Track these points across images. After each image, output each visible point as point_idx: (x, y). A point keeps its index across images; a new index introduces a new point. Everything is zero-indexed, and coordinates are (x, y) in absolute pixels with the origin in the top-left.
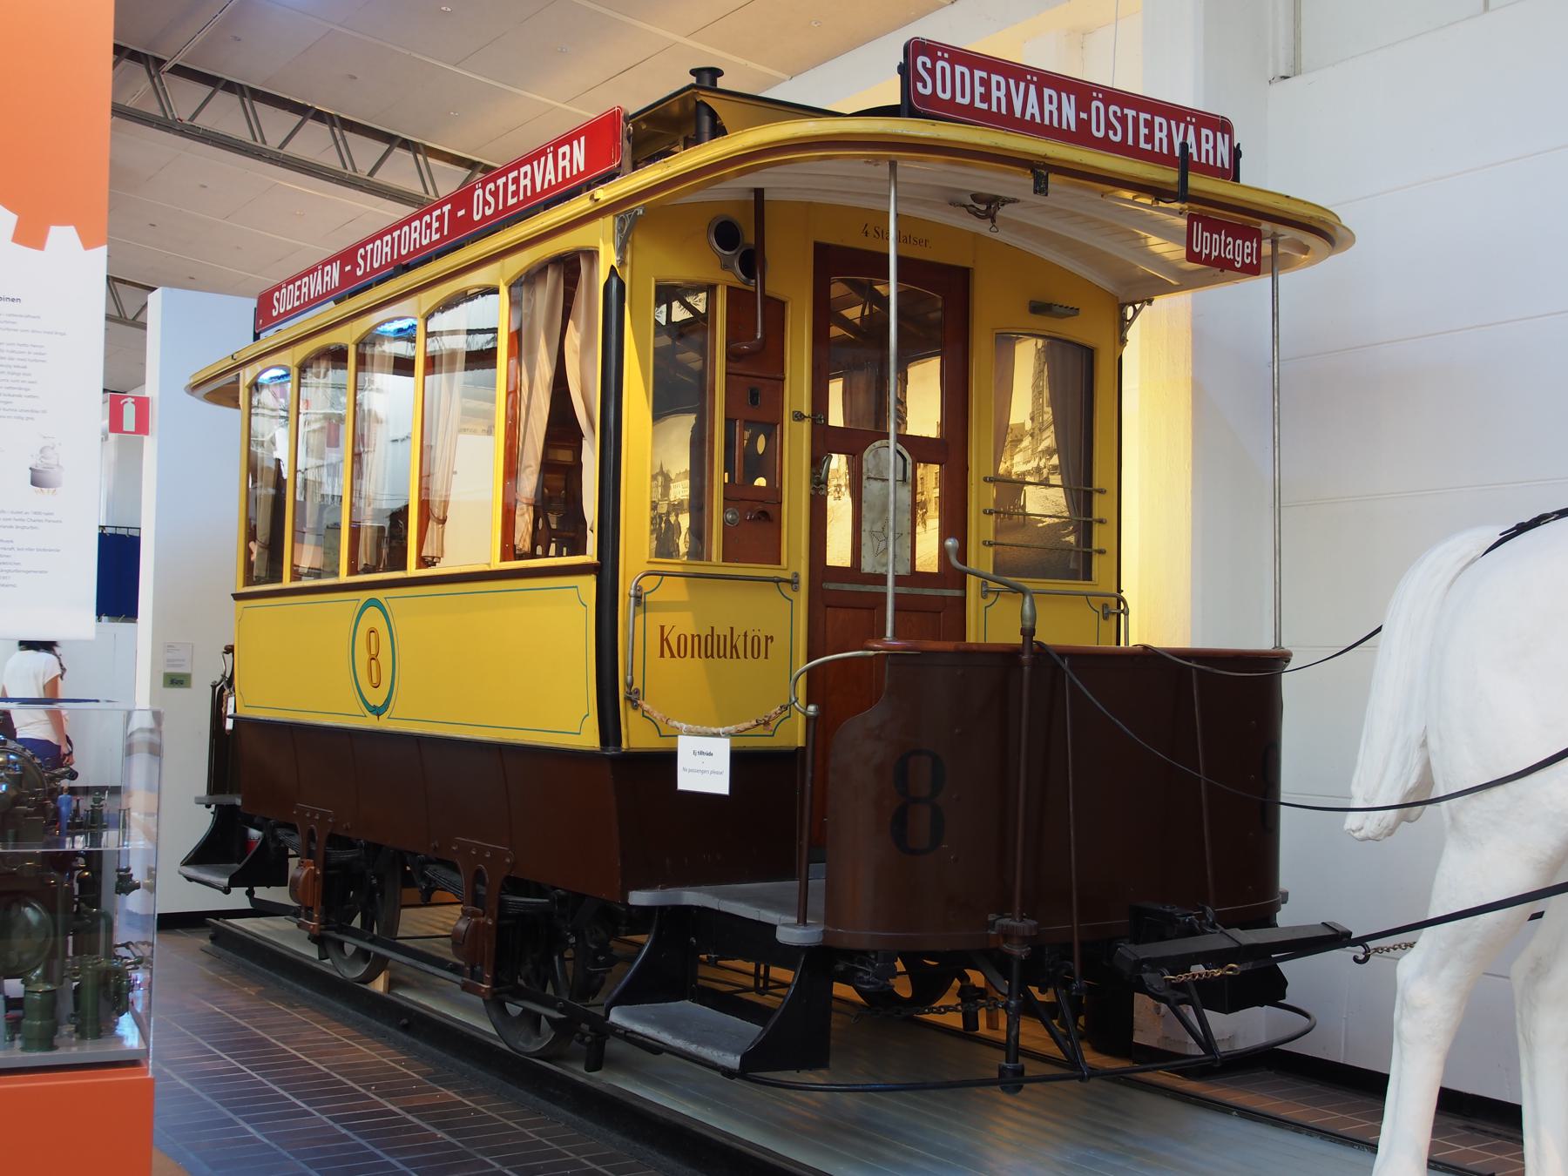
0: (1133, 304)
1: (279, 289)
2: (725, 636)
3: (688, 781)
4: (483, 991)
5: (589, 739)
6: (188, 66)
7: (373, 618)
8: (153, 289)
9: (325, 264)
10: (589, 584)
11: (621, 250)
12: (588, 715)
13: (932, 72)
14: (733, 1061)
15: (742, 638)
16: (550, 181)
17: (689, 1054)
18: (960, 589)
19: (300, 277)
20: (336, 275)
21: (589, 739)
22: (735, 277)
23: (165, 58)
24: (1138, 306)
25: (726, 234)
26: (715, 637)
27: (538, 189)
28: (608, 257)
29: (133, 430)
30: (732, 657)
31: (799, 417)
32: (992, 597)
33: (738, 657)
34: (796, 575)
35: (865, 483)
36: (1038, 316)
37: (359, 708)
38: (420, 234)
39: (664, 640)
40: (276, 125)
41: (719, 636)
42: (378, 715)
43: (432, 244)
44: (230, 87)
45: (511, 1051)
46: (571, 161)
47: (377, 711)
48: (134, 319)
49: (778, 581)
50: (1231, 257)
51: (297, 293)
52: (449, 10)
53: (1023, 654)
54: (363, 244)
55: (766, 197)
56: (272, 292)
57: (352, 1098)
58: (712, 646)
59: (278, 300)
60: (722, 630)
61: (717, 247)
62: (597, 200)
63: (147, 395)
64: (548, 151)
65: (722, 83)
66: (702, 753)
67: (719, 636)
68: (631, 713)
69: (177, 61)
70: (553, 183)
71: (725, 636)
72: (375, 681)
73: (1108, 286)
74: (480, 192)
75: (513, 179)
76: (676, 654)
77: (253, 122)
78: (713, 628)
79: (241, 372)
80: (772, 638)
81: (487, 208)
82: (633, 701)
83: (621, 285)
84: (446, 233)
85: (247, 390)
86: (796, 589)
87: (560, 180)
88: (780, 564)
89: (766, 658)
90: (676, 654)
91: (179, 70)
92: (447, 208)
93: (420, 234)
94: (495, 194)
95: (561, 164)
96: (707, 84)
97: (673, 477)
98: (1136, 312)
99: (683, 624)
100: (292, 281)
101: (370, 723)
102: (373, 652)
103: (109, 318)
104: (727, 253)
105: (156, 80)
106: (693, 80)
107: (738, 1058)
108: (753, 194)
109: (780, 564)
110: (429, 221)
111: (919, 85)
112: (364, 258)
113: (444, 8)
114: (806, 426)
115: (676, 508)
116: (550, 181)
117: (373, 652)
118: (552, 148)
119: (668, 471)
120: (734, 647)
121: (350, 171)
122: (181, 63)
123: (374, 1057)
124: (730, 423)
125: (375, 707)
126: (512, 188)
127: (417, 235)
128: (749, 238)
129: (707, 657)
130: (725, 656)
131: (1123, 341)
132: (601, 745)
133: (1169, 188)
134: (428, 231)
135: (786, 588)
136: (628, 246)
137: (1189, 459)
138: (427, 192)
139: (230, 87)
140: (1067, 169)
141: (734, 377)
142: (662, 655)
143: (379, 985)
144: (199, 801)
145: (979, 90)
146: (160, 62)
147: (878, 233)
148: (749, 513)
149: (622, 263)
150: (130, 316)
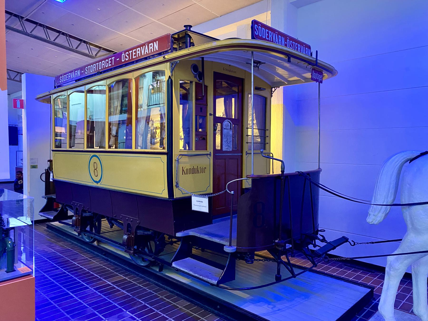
0: (274, 88)
1: (62, 76)
2: (196, 168)
3: (195, 208)
4: (131, 253)
5: (165, 195)
6: (29, 19)
7: (95, 159)
8: (23, 74)
9: (75, 70)
10: (165, 157)
11: (172, 72)
12: (165, 189)
13: (258, 29)
14: (215, 282)
15: (200, 168)
16: (147, 52)
17: (200, 278)
18: (241, 153)
19: (68, 73)
20: (79, 73)
21: (165, 195)
22: (195, 80)
23: (24, 17)
24: (276, 88)
25: (195, 68)
26: (194, 169)
27: (143, 54)
28: (168, 73)
29: (20, 107)
30: (197, 173)
31: (211, 115)
32: (248, 155)
33: (199, 173)
34: (211, 153)
35: (223, 130)
36: (257, 90)
37: (90, 180)
38: (105, 64)
39: (183, 170)
40: (53, 35)
41: (195, 168)
42: (97, 183)
43: (109, 67)
44: (41, 25)
45: (137, 265)
46: (153, 47)
47: (97, 182)
48: (13, 79)
49: (207, 155)
50: (318, 79)
51: (67, 77)
52: (99, 9)
53: (281, 177)
54: (87, 66)
55: (205, 59)
56: (60, 76)
57: (82, 263)
58: (194, 171)
59: (61, 78)
60: (195, 167)
61: (193, 72)
62: (166, 58)
63: (22, 99)
64: (146, 44)
65: (192, 29)
66: (199, 201)
67: (195, 168)
68: (176, 189)
69: (27, 18)
70: (148, 53)
71: (196, 168)
72: (96, 175)
73: (270, 84)
74: (124, 54)
75: (134, 51)
76: (186, 174)
77: (47, 35)
78: (193, 167)
79: (52, 96)
80: (206, 168)
81: (126, 58)
82: (177, 186)
83: (172, 81)
84: (113, 64)
85: (53, 100)
86: (210, 156)
87: (150, 52)
88: (207, 150)
89: (205, 173)
90: (186, 174)
91: (27, 20)
92: (113, 58)
93: (105, 64)
94: (129, 55)
95: (150, 48)
96: (188, 29)
97: (154, 121)
98: (275, 90)
99: (188, 166)
100: (65, 74)
101: (95, 185)
102: (95, 168)
103: (8, 79)
104: (195, 73)
105: (21, 22)
106: (185, 28)
107: (216, 282)
108: (201, 58)
109: (207, 150)
110: (107, 61)
111: (255, 32)
112: (88, 69)
113: (98, 9)
114: (212, 117)
115: (156, 128)
116: (147, 52)
117: (95, 168)
118: (147, 44)
119: (153, 120)
120: (198, 171)
121: (71, 47)
122: (28, 18)
123: (99, 265)
124: (196, 116)
125: (96, 181)
126: (134, 54)
127: (104, 64)
128: (200, 70)
129: (192, 174)
130: (196, 173)
131: (272, 96)
132: (169, 196)
133: (312, 62)
134: (107, 64)
135: (209, 156)
136: (173, 71)
137: (282, 122)
138: (90, 53)
139: (41, 25)
140: (296, 56)
141: (197, 105)
142: (183, 174)
143: (95, 243)
144: (43, 197)
145: (267, 35)
146: (22, 18)
147: (226, 69)
148: (201, 138)
149: (172, 75)
150: (12, 78)
